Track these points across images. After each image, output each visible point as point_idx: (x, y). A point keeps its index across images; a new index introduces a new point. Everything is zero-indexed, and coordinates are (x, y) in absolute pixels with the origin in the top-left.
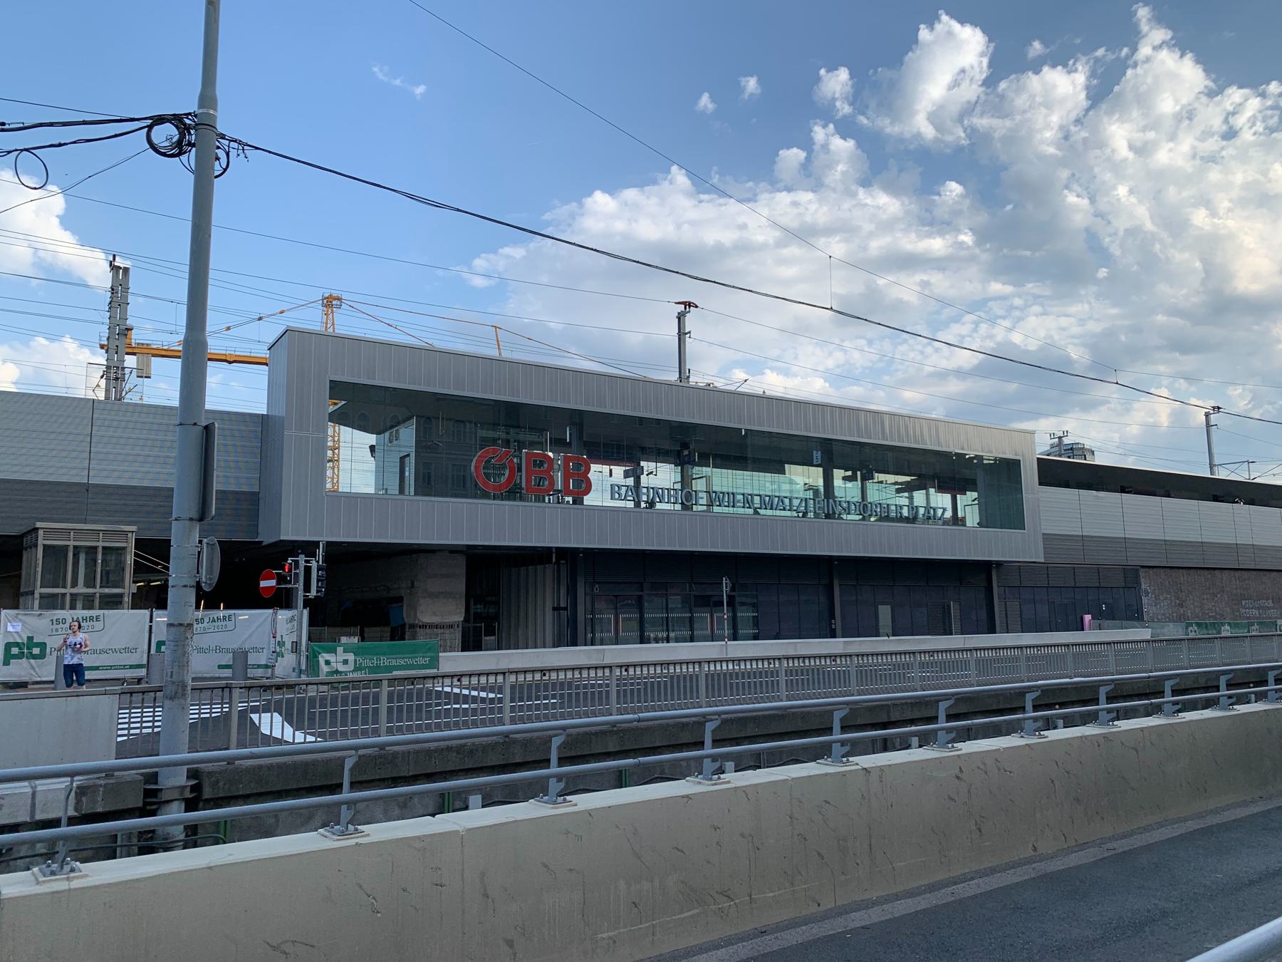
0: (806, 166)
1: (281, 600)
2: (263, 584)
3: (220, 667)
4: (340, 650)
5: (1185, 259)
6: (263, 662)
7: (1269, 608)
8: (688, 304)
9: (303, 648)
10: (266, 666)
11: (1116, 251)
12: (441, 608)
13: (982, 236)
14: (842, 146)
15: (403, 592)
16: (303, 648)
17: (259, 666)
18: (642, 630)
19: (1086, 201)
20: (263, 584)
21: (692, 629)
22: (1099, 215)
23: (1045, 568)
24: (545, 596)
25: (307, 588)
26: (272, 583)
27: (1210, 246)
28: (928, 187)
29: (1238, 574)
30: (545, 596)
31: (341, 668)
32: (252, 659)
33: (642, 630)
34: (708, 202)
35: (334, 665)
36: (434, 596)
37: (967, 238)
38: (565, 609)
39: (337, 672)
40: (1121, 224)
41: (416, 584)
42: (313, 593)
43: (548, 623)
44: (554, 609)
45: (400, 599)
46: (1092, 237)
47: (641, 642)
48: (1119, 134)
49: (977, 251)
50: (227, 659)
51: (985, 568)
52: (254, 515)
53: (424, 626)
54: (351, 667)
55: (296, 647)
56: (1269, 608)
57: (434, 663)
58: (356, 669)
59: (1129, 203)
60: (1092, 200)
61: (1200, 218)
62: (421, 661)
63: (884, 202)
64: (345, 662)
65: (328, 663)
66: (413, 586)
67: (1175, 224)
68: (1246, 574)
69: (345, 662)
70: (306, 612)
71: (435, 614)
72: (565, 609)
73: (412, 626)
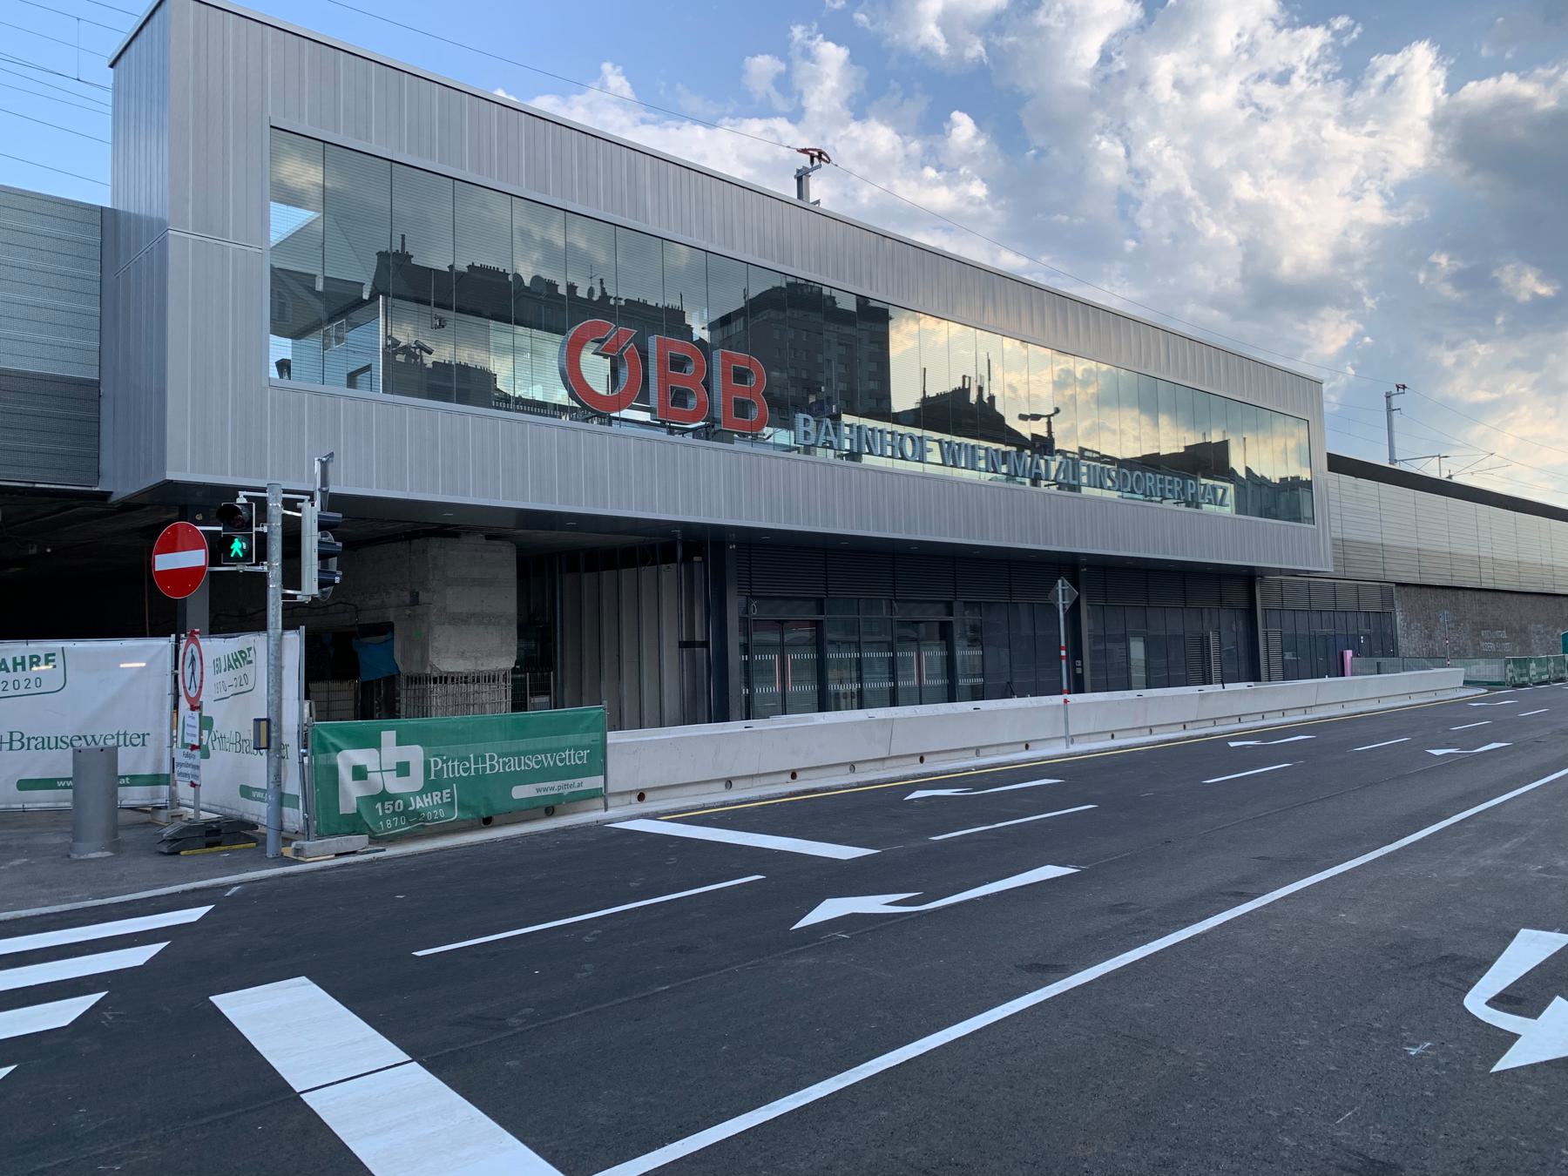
0: (784, 83)
1: (236, 608)
2: (164, 562)
3: (24, 785)
4: (388, 737)
5: (1218, 231)
6: (147, 770)
7: (1504, 640)
8: (818, 156)
9: (290, 736)
10: (156, 779)
11: (1146, 223)
12: (471, 644)
13: (998, 188)
14: (832, 55)
15: (391, 615)
16: (290, 736)
17: (135, 780)
18: (822, 681)
19: (1121, 151)
20: (164, 562)
21: (894, 678)
22: (1137, 174)
23: (1332, 585)
24: (660, 623)
25: (292, 577)
26: (195, 558)
27: (1257, 215)
28: (934, 125)
29: (1478, 595)
30: (660, 623)
31: (395, 785)
32: (127, 762)
33: (822, 681)
34: (654, 123)
35: (375, 777)
36: (459, 620)
37: (978, 190)
38: (705, 644)
39: (384, 796)
40: (1158, 185)
41: (423, 597)
42: (310, 587)
43: (670, 674)
44: (682, 645)
45: (386, 628)
46: (1125, 202)
47: (822, 707)
48: (1165, 66)
49: (988, 208)
50: (60, 764)
51: (1247, 578)
52: (90, 432)
53: (443, 679)
54: (416, 781)
55: (266, 734)
56: (1504, 640)
57: (598, 762)
58: (431, 786)
59: (1168, 160)
60: (1128, 154)
61: (1243, 188)
62: (573, 758)
63: (881, 137)
64: (403, 769)
65: (359, 773)
66: (415, 601)
67: (1213, 189)
68: (1483, 595)
69: (403, 769)
70: (294, 643)
71: (462, 655)
72: (705, 644)
73: (416, 680)
